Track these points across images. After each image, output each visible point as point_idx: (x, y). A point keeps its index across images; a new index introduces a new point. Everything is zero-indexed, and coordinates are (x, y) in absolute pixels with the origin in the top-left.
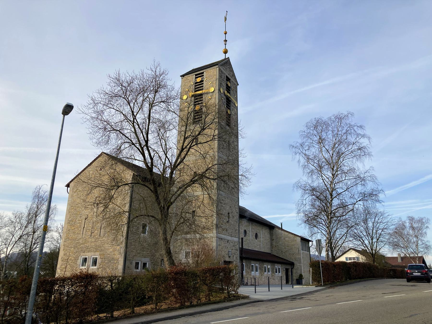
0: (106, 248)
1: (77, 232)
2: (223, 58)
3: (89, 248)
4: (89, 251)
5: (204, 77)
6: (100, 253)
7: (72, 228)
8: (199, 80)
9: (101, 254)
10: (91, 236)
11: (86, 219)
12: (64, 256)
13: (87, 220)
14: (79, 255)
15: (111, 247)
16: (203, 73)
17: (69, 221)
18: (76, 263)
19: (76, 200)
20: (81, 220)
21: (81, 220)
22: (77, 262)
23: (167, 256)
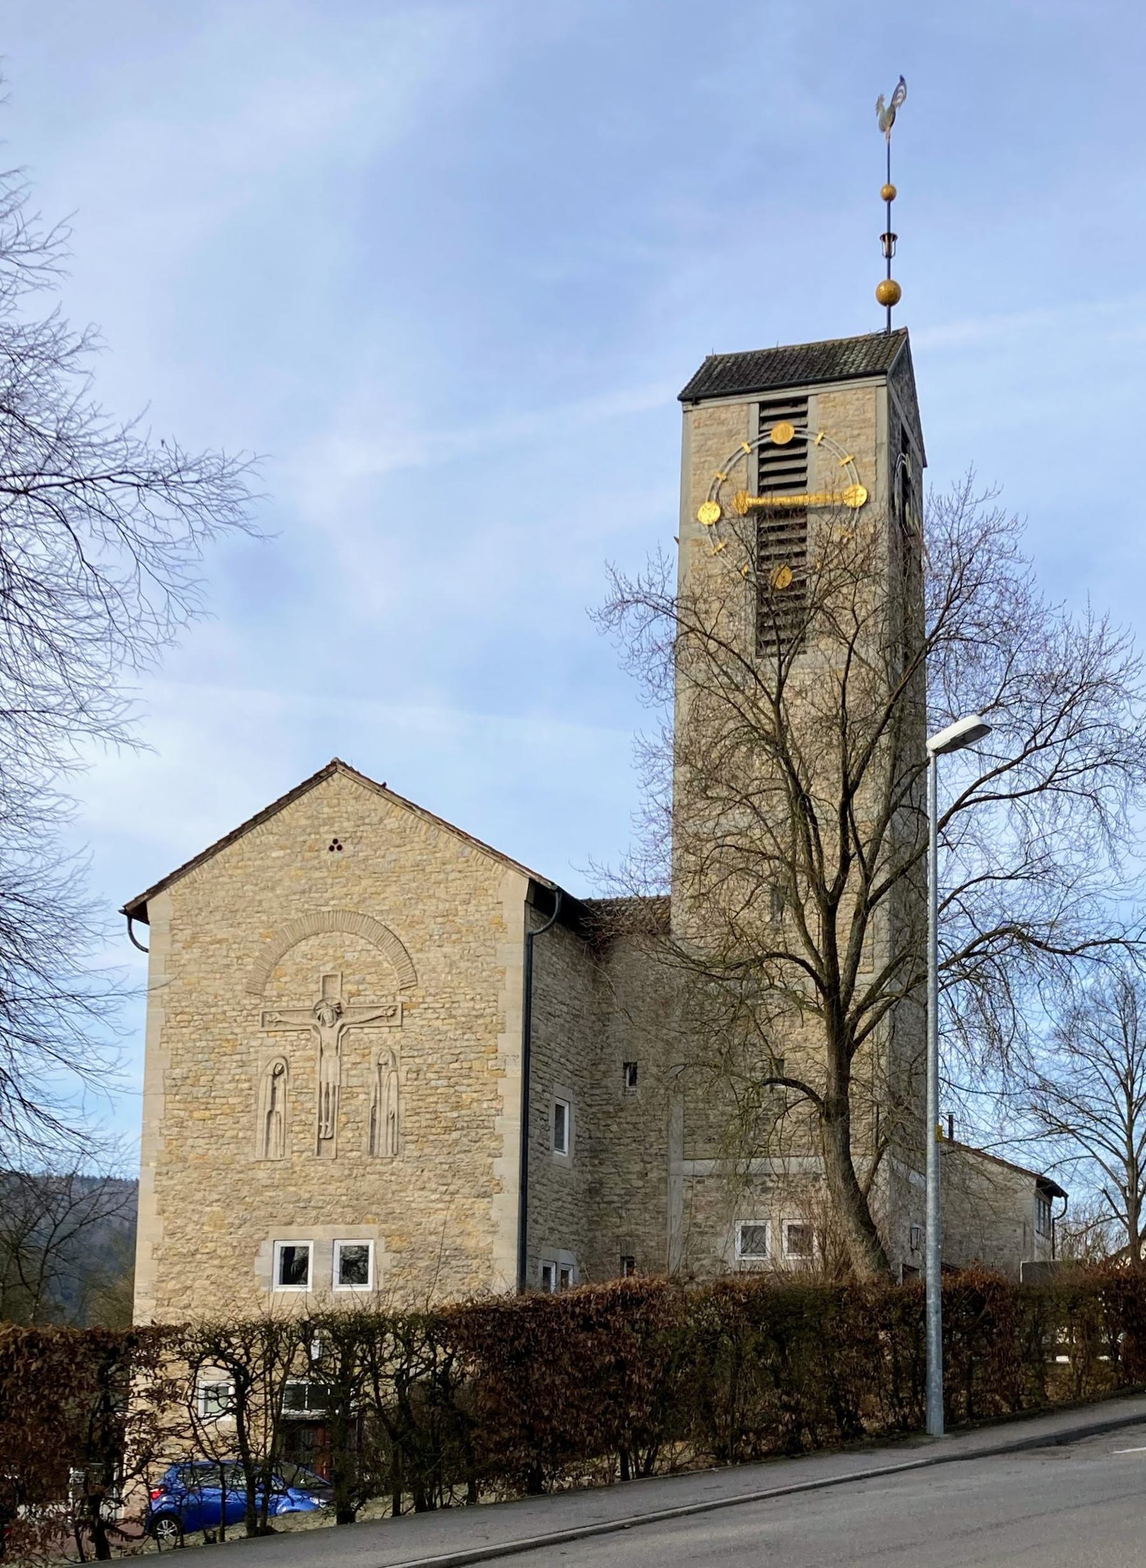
0: (413, 1205)
1: (229, 1134)
2: (880, 326)
3: (312, 1204)
4: (317, 1218)
5: (809, 419)
6: (384, 1226)
7: (196, 1115)
8: (782, 432)
9: (387, 1233)
10: (319, 1153)
11: (275, 1076)
12: (167, 1239)
13: (285, 1082)
14: (262, 1235)
15: (439, 1201)
16: (804, 400)
17: (168, 1082)
18: (245, 1269)
19: (204, 983)
20: (249, 1080)
21: (249, 1080)
22: (252, 1264)
23: (864, 1236)
